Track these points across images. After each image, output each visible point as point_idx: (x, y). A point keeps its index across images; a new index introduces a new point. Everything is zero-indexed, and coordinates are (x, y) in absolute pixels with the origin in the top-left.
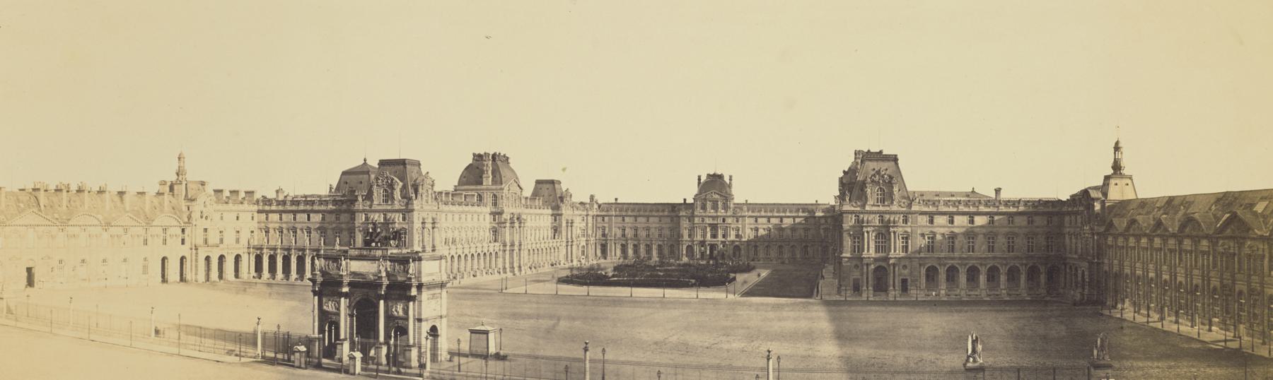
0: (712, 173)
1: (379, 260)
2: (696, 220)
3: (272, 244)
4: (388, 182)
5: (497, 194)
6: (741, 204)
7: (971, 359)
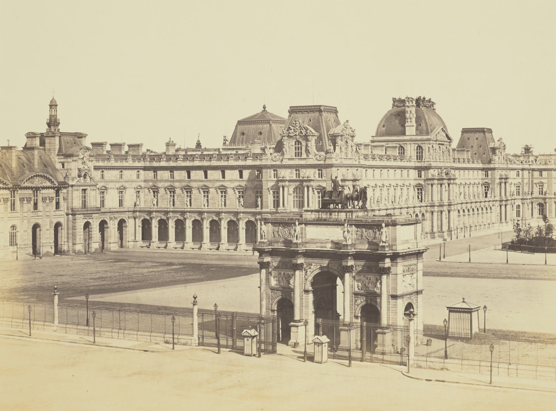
1: (343, 225)
3: (163, 206)
4: (301, 132)
5: (423, 146)
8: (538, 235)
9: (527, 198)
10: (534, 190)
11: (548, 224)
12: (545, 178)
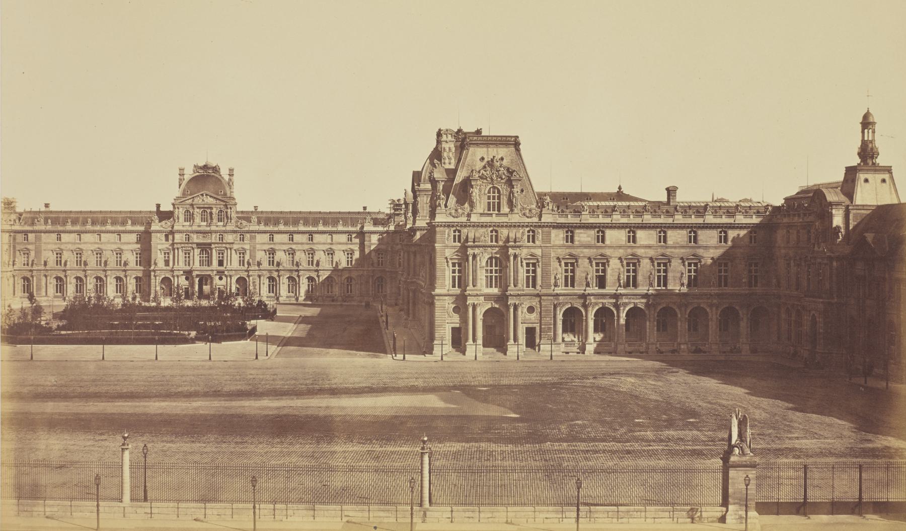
2: (178, 238)
6: (247, 212)
7: (737, 451)
8: (21, 321)
9: (6, 270)
10: (16, 260)
11: (35, 305)
12: (32, 243)
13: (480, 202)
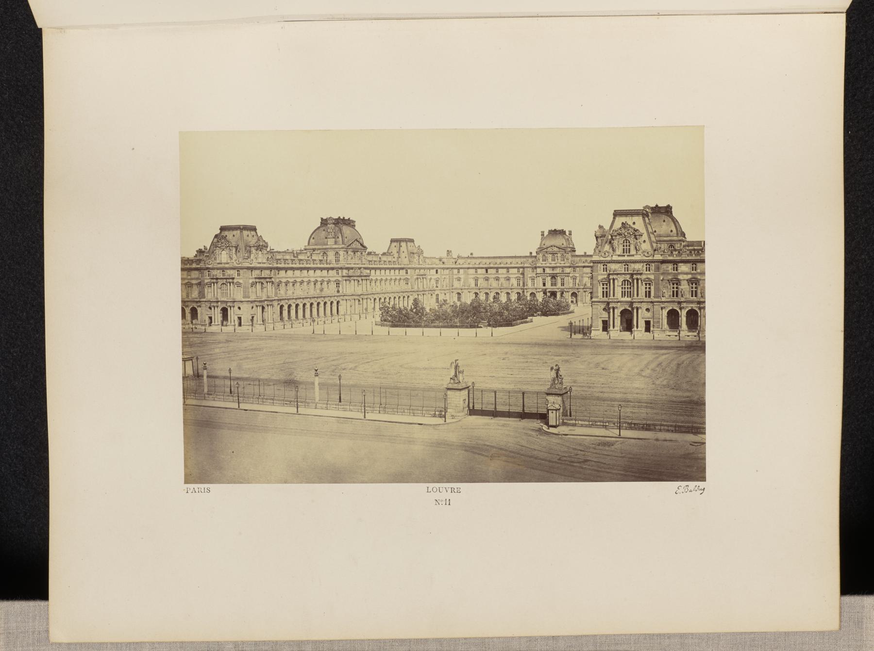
0: (550, 229)
13: (618, 249)
